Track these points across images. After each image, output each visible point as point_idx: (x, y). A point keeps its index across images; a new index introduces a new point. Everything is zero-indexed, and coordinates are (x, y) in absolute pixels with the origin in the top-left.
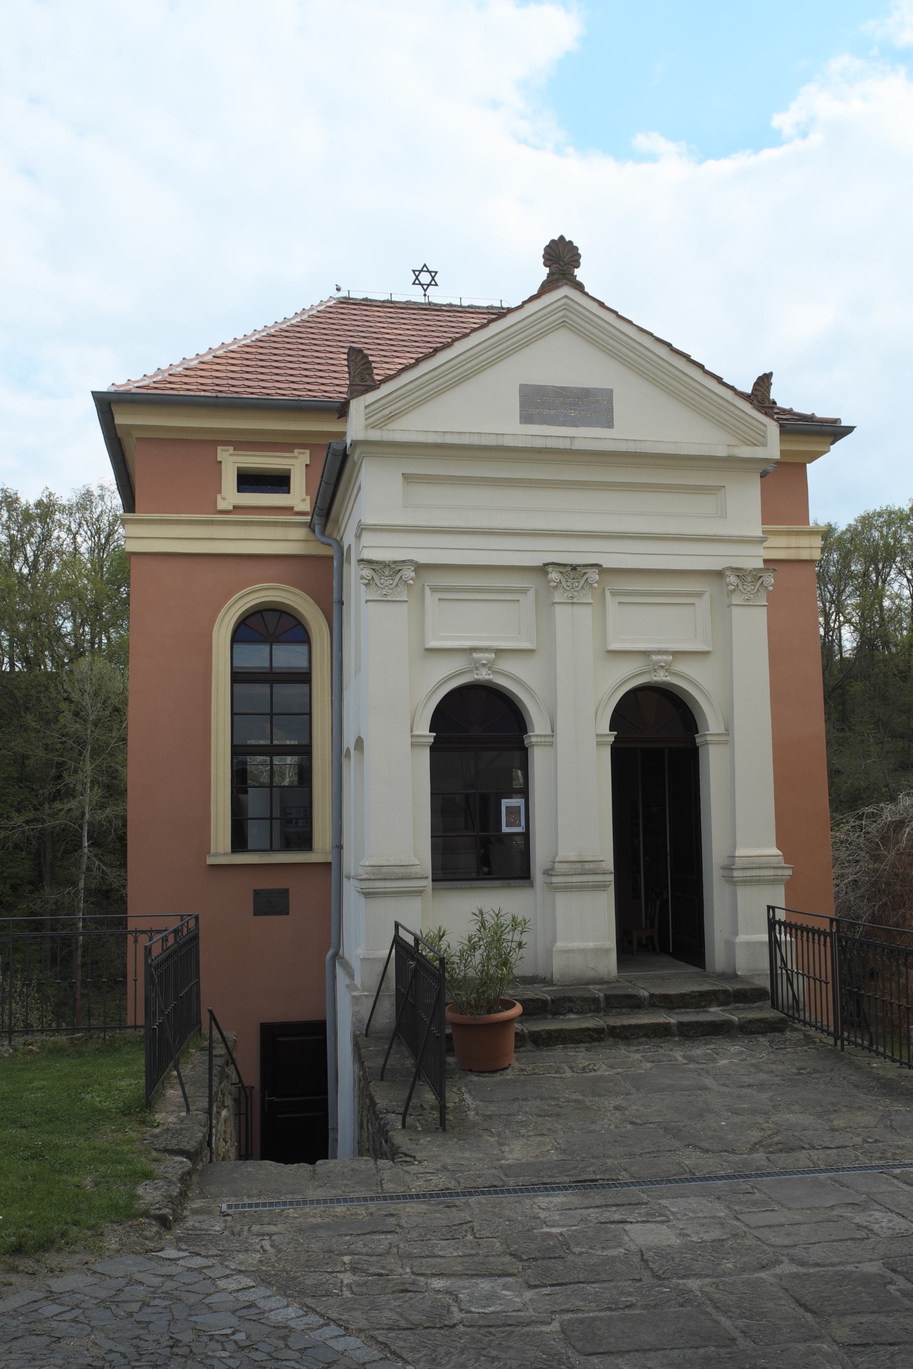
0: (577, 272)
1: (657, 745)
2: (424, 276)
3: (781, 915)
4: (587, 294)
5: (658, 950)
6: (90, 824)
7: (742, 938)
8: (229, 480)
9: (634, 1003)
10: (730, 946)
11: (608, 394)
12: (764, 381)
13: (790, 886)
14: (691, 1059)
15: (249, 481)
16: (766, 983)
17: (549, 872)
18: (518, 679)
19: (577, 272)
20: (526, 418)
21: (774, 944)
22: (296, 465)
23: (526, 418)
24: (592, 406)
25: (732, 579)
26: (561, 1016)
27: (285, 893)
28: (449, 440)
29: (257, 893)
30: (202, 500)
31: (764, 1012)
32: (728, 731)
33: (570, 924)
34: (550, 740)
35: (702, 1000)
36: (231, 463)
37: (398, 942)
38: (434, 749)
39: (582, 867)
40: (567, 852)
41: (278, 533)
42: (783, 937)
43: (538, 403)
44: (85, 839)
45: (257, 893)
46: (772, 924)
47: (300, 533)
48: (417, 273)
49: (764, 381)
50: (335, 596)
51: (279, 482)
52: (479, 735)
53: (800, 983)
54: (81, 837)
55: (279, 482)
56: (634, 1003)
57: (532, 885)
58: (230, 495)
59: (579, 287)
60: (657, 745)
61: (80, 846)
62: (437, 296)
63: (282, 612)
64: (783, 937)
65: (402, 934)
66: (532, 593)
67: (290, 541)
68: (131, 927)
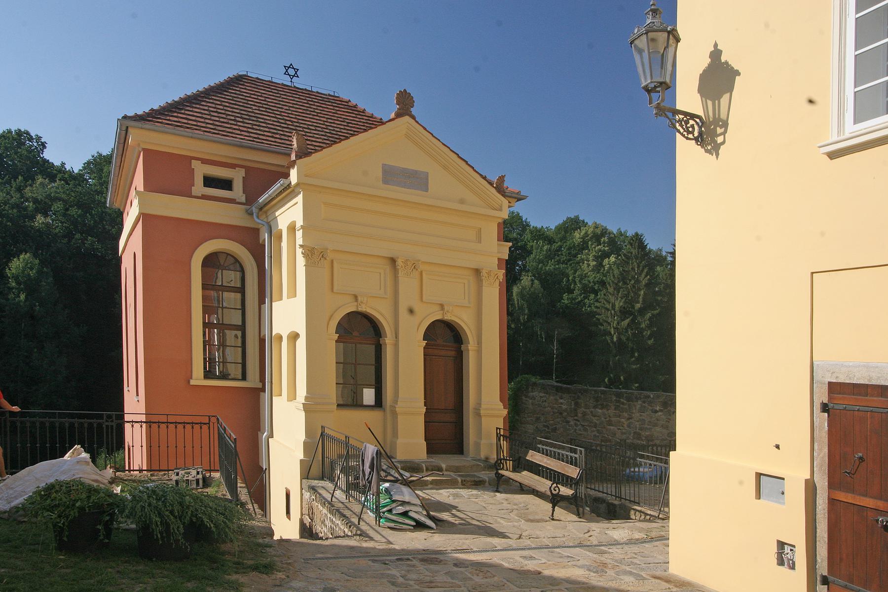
0: (412, 109)
1: (445, 339)
2: (291, 70)
4: (417, 122)
5: (858, 16)
8: (199, 181)
10: (478, 445)
11: (426, 175)
12: (502, 179)
15: (210, 182)
18: (380, 311)
19: (412, 109)
22: (237, 177)
36: (200, 171)
46: (498, 437)
48: (287, 68)
49: (502, 179)
55: (226, 184)
58: (199, 187)
59: (414, 118)
60: (445, 339)
62: (298, 83)
63: (228, 254)
68: (127, 418)
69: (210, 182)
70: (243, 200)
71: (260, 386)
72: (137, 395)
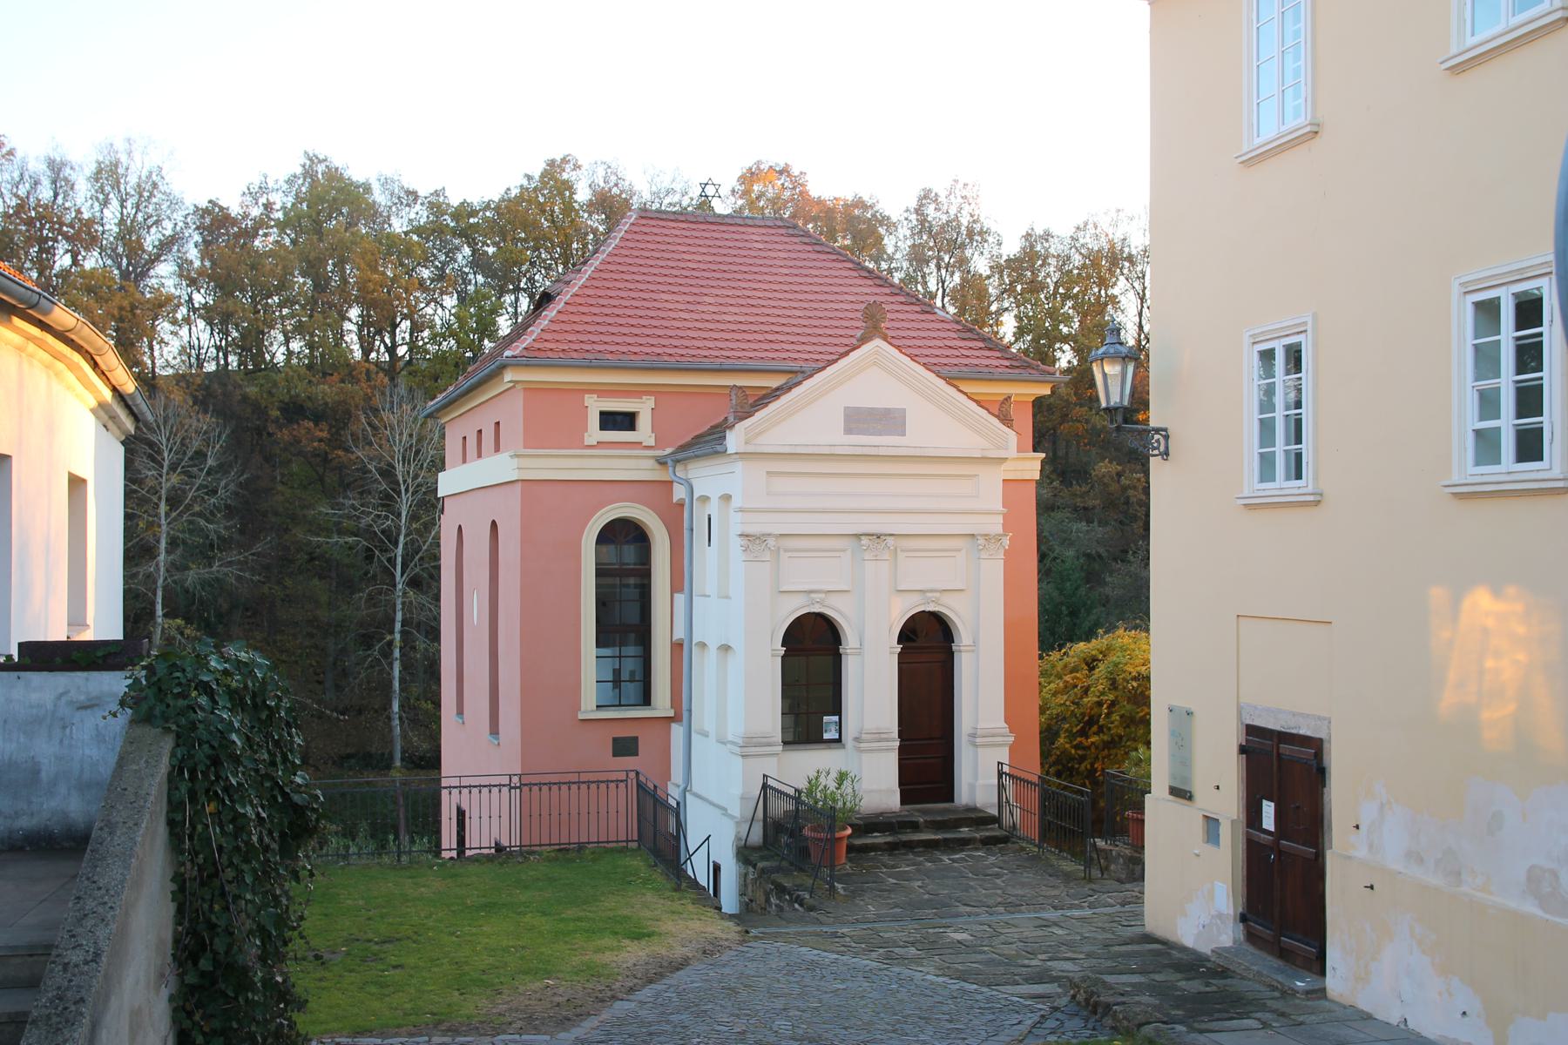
1: (927, 643)
3: (1006, 769)
6: (165, 588)
7: (981, 782)
8: (594, 420)
9: (915, 826)
10: (972, 787)
13: (1013, 749)
14: (954, 861)
15: (611, 420)
16: (995, 812)
17: (857, 739)
18: (837, 610)
20: (848, 431)
21: (1001, 787)
23: (848, 431)
24: (890, 420)
25: (981, 541)
26: (878, 838)
27: (635, 739)
28: (799, 450)
29: (615, 740)
30: (572, 439)
31: (992, 831)
32: (975, 643)
33: (866, 768)
34: (860, 651)
35: (956, 824)
36: (595, 406)
37: (765, 787)
38: (901, 749)
39: (879, 736)
40: (870, 725)
41: (632, 463)
42: (1007, 781)
43: (858, 420)
44: (159, 607)
45: (615, 740)
46: (1000, 774)
47: (651, 463)
50: (686, 525)
51: (626, 421)
52: (812, 649)
53: (1017, 812)
54: (153, 604)
55: (626, 421)
56: (915, 826)
57: (844, 747)
58: (594, 433)
60: (927, 643)
61: (152, 614)
64: (1007, 781)
65: (770, 782)
66: (849, 552)
67: (641, 468)
69: (611, 420)
70: (652, 442)
71: (671, 713)
72: (494, 730)
